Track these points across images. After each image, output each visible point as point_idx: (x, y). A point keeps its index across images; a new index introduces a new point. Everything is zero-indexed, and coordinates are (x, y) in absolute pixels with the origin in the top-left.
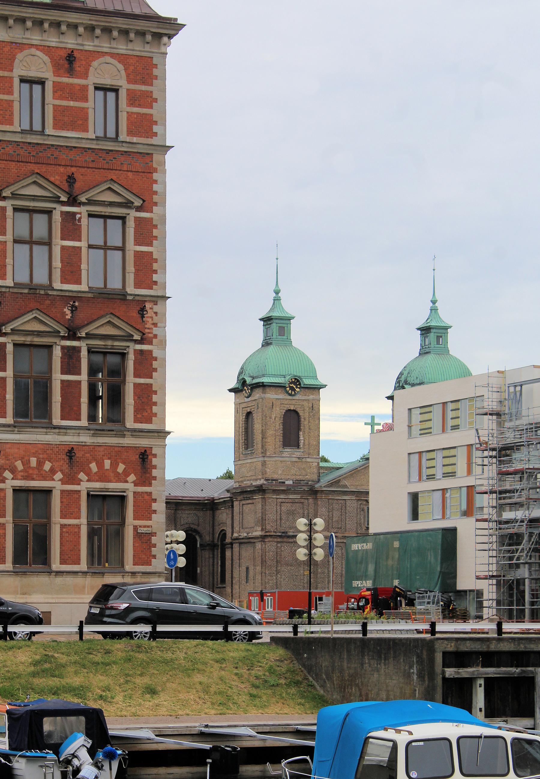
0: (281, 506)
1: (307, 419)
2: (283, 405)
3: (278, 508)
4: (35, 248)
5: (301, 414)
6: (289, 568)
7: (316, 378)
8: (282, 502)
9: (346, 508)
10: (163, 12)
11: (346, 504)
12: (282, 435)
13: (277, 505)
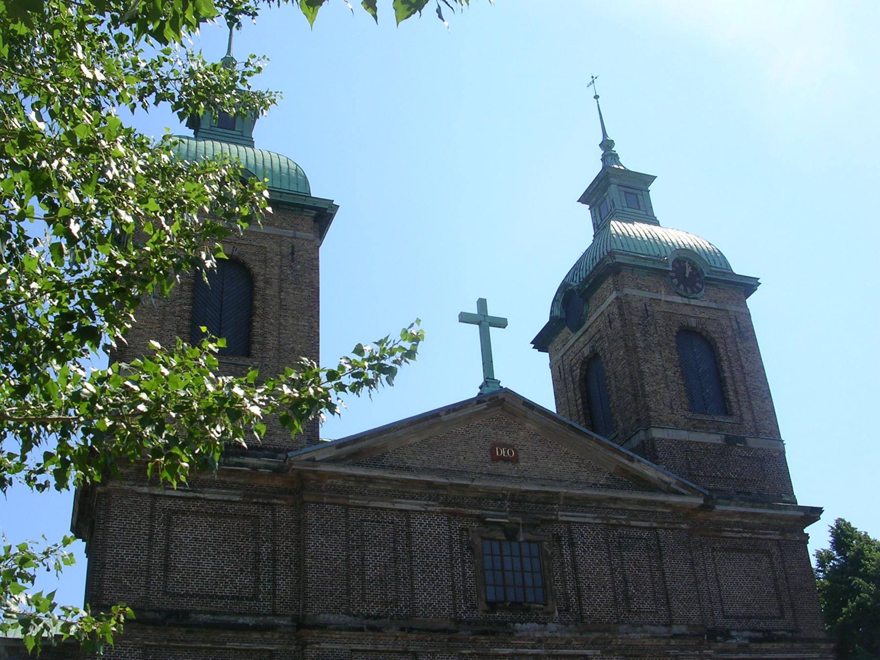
0: (168, 522)
1: (275, 282)
3: (159, 527)
5: (256, 270)
8: (175, 512)
9: (409, 536)
11: (408, 525)
12: (187, 315)
13: (151, 517)
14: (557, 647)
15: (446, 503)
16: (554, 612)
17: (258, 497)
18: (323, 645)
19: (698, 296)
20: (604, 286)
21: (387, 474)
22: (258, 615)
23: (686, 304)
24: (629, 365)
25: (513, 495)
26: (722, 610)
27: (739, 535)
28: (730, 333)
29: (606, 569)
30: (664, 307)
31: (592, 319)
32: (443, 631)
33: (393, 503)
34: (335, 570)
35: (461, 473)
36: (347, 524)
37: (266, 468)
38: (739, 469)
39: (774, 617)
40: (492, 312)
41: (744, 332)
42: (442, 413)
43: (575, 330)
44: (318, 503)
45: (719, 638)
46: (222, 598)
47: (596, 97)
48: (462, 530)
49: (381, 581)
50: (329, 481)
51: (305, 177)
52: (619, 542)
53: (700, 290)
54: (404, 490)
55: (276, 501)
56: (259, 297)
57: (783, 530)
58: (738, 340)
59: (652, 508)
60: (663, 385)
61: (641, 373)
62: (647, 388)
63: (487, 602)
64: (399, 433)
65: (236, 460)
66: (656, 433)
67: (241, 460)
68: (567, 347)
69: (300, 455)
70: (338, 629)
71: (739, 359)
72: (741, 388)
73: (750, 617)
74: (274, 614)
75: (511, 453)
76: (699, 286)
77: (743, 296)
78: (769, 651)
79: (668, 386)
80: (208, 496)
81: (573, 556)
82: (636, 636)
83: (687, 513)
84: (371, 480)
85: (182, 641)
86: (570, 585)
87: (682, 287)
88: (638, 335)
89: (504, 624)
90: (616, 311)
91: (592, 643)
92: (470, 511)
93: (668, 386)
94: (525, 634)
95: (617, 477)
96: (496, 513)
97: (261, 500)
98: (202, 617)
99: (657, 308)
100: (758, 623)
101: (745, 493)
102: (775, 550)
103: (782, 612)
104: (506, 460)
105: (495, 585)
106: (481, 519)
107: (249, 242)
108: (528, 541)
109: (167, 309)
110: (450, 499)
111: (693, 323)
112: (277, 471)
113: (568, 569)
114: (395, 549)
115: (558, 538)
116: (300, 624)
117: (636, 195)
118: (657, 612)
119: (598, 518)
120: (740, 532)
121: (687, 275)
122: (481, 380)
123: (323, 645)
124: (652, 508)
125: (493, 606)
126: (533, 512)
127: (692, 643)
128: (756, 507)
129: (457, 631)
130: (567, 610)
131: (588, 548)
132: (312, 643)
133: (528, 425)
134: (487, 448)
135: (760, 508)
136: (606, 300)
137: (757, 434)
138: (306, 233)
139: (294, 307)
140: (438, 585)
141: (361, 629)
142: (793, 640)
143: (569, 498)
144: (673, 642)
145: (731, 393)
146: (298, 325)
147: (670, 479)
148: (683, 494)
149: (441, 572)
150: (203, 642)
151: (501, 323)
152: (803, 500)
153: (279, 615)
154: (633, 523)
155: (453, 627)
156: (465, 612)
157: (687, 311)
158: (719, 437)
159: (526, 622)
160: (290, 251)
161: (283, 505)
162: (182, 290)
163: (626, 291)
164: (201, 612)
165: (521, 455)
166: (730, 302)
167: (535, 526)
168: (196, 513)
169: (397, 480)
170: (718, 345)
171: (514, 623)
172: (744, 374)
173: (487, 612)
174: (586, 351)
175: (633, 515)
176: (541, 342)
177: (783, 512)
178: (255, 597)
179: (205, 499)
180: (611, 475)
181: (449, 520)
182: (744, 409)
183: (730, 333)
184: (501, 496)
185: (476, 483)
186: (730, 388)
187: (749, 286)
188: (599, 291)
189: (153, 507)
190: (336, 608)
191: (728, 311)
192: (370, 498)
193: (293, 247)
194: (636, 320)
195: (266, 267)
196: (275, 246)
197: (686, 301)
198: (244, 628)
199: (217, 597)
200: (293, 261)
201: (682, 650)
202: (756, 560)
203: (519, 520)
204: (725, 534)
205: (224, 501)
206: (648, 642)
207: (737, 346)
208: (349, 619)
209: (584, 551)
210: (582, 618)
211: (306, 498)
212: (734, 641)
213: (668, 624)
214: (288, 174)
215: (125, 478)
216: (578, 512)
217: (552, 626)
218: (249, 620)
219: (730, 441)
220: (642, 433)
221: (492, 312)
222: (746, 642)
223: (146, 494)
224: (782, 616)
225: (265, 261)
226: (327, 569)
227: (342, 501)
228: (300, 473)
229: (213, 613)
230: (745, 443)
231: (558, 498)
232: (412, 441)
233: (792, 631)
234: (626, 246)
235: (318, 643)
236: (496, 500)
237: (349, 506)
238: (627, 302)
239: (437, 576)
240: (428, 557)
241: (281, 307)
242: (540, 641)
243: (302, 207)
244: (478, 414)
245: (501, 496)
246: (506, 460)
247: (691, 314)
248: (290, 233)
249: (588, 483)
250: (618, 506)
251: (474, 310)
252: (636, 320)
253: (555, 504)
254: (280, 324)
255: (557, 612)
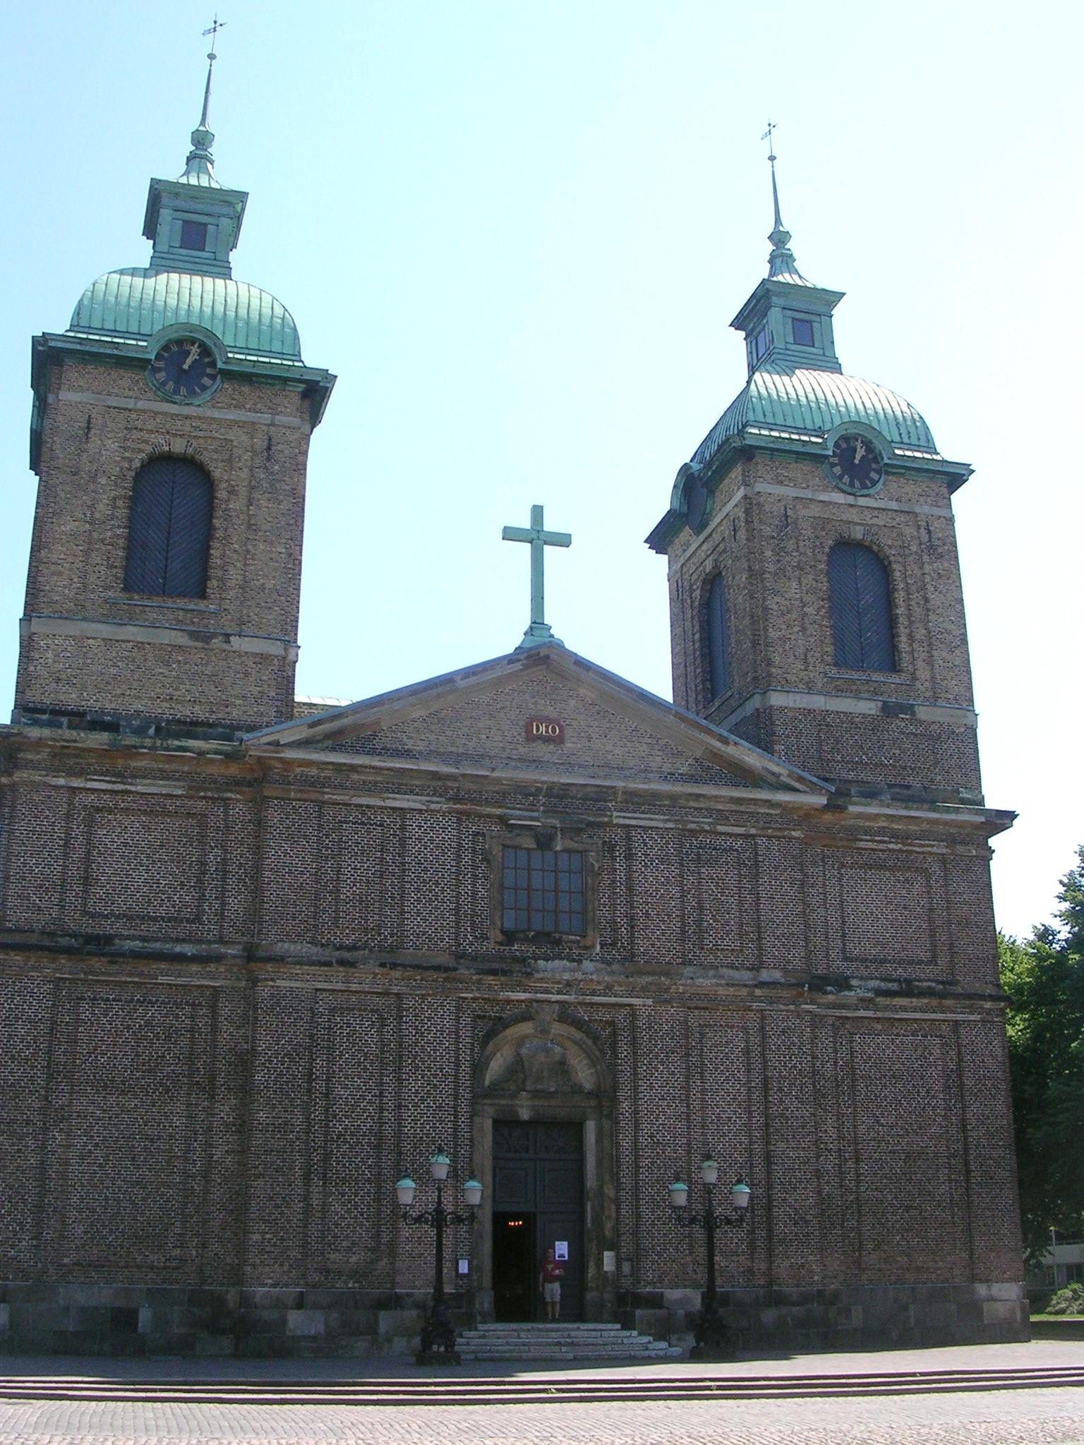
0: (90, 823)
1: (243, 491)
2: (136, 435)
3: (78, 830)
4: (567, 889)
5: (217, 474)
6: (112, 1100)
7: (297, 355)
8: (98, 810)
9: (402, 842)
10: (839, 352)
11: (403, 828)
12: (121, 542)
13: (68, 816)
14: (593, 993)
15: (457, 799)
16: (593, 947)
17: (209, 789)
18: (279, 983)
19: (871, 491)
20: (732, 475)
21: (376, 762)
22: (200, 942)
23: (851, 505)
24: (752, 598)
25: (550, 789)
26: (844, 950)
27: (882, 846)
28: (914, 548)
29: (675, 891)
30: (815, 510)
31: (717, 520)
32: (437, 968)
33: (384, 799)
34: (301, 887)
35: (478, 759)
36: (320, 826)
37: (216, 753)
38: (897, 752)
39: (920, 963)
40: (550, 525)
41: (941, 548)
42: (458, 678)
43: (698, 530)
44: (283, 799)
45: (829, 988)
46: (155, 919)
47: (772, 158)
48: (476, 834)
49: (361, 902)
50: (298, 770)
51: (295, 329)
52: (698, 854)
53: (874, 483)
54: (399, 782)
55: (229, 795)
56: (219, 513)
57: (952, 841)
58: (926, 558)
59: (752, 808)
60: (796, 629)
61: (766, 609)
62: (773, 634)
63: (502, 932)
64: (396, 706)
65: (177, 743)
66: (777, 699)
67: (183, 744)
68: (688, 554)
69: (258, 738)
70: (301, 963)
71: (923, 587)
72: (920, 633)
73: (884, 961)
74: (221, 940)
75: (554, 730)
76: (874, 475)
77: (945, 491)
78: (895, 1009)
79: (804, 629)
80: (140, 789)
81: (629, 871)
82: (705, 983)
83: (806, 816)
84: (354, 768)
85: (103, 974)
86: (621, 910)
87: (846, 479)
88: (768, 553)
89: (522, 961)
90: (742, 516)
91: (643, 989)
92: (489, 810)
93: (804, 629)
94: (549, 975)
95: (706, 763)
96: (526, 813)
97: (210, 794)
98: (129, 944)
99: (804, 512)
100: (896, 970)
101: (902, 786)
102: (936, 868)
103: (935, 956)
104: (547, 740)
105: (516, 909)
106: (502, 820)
107: (209, 434)
108: (567, 851)
109: (94, 534)
110: (463, 796)
111: (858, 533)
112: (230, 757)
113: (621, 889)
114: (382, 859)
115: (611, 848)
116: (251, 955)
117: (810, 322)
118: (741, 951)
119: (668, 820)
120: (885, 842)
121: (857, 461)
122: (527, 623)
123: (279, 983)
124: (752, 808)
125: (510, 936)
126: (578, 814)
127: (785, 994)
128: (911, 809)
129: (455, 969)
130: (613, 944)
131: (652, 861)
132: (266, 980)
133: (582, 691)
134: (521, 723)
135: (917, 809)
136: (729, 502)
137: (934, 700)
138: (290, 418)
139: (268, 526)
140: (437, 908)
141: (329, 964)
142: (942, 996)
143: (629, 794)
144: (758, 992)
145: (903, 639)
146: (270, 552)
147: (779, 768)
148: (797, 790)
149: (443, 890)
150: (131, 974)
151: (563, 541)
152: (994, 799)
153: (227, 942)
154: (720, 828)
155: (452, 964)
156: (471, 944)
157: (852, 515)
158: (872, 705)
159: (553, 959)
160: (266, 443)
161: (238, 800)
162: (115, 507)
163: (759, 487)
164: (128, 938)
165: (568, 732)
166: (922, 499)
167: (579, 831)
168: (126, 810)
169: (390, 769)
170: (894, 566)
171: (536, 960)
172: (928, 610)
173: (501, 944)
174: (709, 566)
175: (723, 817)
176: (660, 539)
177: (952, 817)
178: (197, 919)
179: (138, 793)
180: (696, 760)
181: (459, 821)
182: (920, 663)
183: (914, 548)
184: (533, 790)
185: (496, 774)
186: (902, 631)
187: (955, 476)
188: (726, 481)
189: (70, 803)
190: (299, 935)
191: (916, 515)
192: (352, 792)
193: (270, 439)
194: (767, 531)
195: (232, 469)
196: (244, 438)
197: (851, 500)
198: (182, 958)
199: (151, 918)
200: (268, 459)
201: (771, 1003)
202: (907, 880)
203: (557, 823)
204: (862, 844)
205: (162, 795)
206: (721, 991)
207: (921, 568)
208: (314, 949)
209: (646, 866)
210: (633, 956)
211: (267, 793)
212: (852, 993)
213: (755, 969)
214: (271, 326)
215: (35, 766)
216: (643, 813)
217: (587, 965)
218: (188, 949)
219: (889, 710)
220: (757, 697)
221: (550, 525)
222: (870, 995)
223: (62, 787)
224: (933, 961)
225: (230, 461)
226: (290, 886)
227: (314, 796)
228: (260, 759)
229: (144, 939)
230: (913, 713)
231: (615, 794)
232: (416, 715)
233: (943, 983)
234: (769, 415)
235: (272, 980)
236: (527, 795)
237: (323, 803)
238: (758, 504)
239: (436, 895)
240: (425, 870)
241: (249, 526)
242: (568, 984)
243: (285, 380)
244: (514, 675)
245: (533, 790)
246: (547, 740)
247: (857, 520)
248: (266, 418)
249: (662, 772)
250: (701, 805)
251: (525, 523)
252: (767, 531)
253: (611, 801)
254: (248, 551)
255: (598, 947)
